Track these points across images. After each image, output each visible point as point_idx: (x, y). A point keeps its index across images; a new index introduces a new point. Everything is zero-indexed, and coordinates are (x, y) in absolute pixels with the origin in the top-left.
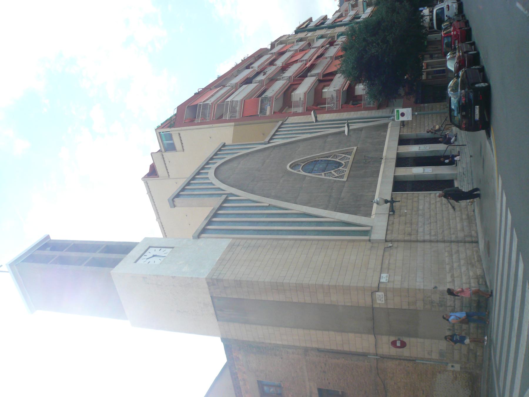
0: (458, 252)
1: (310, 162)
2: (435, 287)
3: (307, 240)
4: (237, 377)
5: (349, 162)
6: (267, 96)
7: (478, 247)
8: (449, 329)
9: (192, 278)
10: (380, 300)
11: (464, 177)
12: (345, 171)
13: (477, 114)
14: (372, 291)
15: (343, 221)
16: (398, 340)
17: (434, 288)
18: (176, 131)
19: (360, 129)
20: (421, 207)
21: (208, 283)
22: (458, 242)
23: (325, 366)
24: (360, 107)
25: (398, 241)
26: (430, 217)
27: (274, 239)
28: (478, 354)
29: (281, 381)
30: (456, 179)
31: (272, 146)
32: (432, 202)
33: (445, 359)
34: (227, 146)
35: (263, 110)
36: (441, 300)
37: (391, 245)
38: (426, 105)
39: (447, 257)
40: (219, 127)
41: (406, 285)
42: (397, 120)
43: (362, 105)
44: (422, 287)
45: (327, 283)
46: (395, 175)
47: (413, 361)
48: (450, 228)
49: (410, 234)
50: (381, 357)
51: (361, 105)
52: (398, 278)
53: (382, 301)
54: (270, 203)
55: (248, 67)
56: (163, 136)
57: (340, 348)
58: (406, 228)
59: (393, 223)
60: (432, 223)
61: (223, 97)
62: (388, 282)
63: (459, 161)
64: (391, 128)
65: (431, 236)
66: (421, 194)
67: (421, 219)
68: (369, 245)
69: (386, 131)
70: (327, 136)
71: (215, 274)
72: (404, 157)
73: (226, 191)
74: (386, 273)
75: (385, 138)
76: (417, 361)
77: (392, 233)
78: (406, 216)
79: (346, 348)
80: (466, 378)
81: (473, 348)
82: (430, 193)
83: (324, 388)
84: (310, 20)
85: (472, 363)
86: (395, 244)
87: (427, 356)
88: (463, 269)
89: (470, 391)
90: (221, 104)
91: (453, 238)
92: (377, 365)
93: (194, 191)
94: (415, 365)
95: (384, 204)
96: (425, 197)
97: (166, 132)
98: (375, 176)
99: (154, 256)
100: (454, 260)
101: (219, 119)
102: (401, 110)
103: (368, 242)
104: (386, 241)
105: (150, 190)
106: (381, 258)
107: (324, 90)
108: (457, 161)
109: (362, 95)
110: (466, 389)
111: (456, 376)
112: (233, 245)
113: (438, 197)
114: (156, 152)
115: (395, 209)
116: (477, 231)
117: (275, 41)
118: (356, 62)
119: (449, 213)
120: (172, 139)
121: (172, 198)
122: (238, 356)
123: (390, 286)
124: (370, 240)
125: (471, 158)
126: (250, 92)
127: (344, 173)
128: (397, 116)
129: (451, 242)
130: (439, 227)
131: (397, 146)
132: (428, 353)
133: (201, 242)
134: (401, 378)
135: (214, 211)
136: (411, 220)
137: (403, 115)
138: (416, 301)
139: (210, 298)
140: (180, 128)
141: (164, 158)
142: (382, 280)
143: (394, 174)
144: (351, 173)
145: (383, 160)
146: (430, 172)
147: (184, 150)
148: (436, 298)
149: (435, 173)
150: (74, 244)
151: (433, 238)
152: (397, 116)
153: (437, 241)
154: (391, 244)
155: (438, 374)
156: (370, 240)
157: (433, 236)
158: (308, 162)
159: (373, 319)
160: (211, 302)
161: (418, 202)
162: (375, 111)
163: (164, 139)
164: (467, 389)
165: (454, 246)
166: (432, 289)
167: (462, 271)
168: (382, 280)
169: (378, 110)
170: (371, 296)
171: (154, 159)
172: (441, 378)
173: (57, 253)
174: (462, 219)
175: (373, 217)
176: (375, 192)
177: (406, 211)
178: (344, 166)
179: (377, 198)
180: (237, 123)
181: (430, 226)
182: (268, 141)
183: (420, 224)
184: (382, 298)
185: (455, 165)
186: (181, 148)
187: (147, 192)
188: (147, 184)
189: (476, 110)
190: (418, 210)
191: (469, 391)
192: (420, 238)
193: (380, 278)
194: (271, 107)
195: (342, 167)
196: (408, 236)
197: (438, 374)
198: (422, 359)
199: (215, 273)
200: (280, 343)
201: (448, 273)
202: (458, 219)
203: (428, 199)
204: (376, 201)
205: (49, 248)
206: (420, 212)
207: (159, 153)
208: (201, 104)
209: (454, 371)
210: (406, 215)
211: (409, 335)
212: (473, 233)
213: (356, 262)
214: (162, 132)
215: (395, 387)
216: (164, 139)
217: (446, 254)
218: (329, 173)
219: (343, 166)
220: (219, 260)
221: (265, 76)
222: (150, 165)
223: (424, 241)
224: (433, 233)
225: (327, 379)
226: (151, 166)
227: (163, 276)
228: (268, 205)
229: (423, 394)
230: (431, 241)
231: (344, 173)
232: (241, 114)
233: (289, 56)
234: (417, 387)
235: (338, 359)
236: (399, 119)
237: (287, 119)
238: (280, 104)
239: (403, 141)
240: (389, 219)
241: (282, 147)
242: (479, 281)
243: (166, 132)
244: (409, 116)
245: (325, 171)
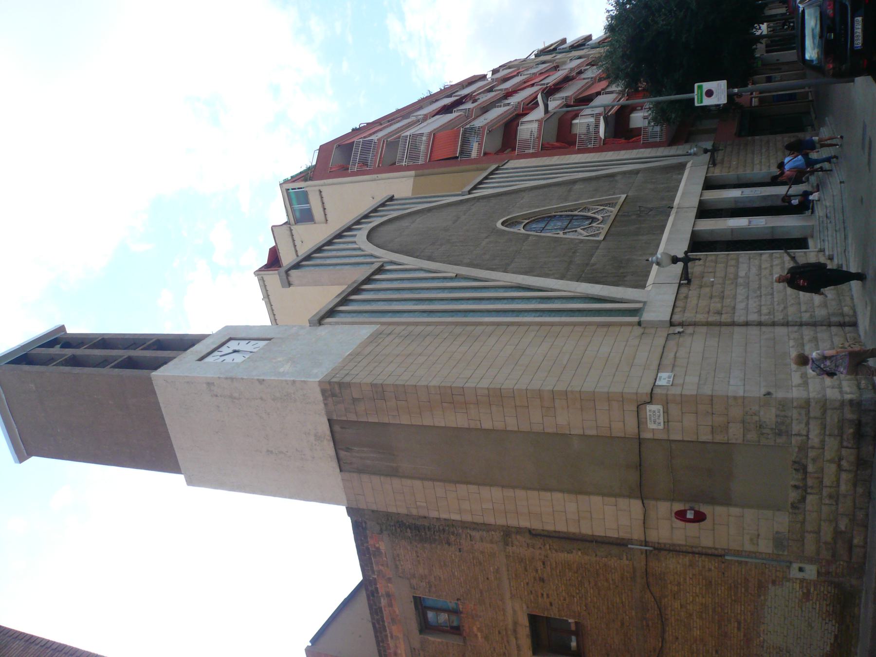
1: (540, 218)
2: (769, 394)
3: (519, 324)
4: (377, 589)
6: (473, 125)
7: (857, 331)
8: (796, 487)
9: (294, 382)
10: (655, 422)
11: (829, 222)
12: (602, 229)
13: (858, 34)
14: (639, 403)
15: (590, 296)
16: (689, 510)
17: (765, 395)
18: (315, 186)
20: (742, 273)
21: (323, 392)
23: (544, 568)
24: (637, 141)
27: (457, 324)
28: (856, 541)
29: (458, 600)
30: (812, 237)
32: (763, 266)
33: (786, 553)
34: (397, 200)
35: (465, 152)
36: (779, 420)
37: (681, 330)
38: (757, 137)
39: (793, 347)
40: (389, 179)
41: (707, 390)
42: (698, 103)
43: (641, 138)
44: (741, 393)
45: (550, 388)
46: (694, 229)
47: (720, 558)
48: (799, 304)
49: (719, 313)
50: (655, 548)
51: (639, 139)
55: (450, 96)
56: (293, 196)
57: (573, 529)
58: (712, 305)
59: (686, 297)
60: (763, 297)
62: (672, 385)
63: (818, 202)
64: (690, 169)
65: (761, 315)
68: (638, 331)
69: (683, 174)
70: (574, 182)
71: (337, 375)
72: (713, 208)
73: (382, 258)
76: (727, 558)
77: (684, 310)
78: (713, 286)
79: (586, 529)
80: (829, 595)
81: (846, 528)
82: (761, 254)
83: (542, 615)
84: (564, 41)
85: (842, 563)
86: (690, 330)
87: (748, 547)
89: (837, 625)
90: (392, 144)
91: (806, 317)
92: (646, 565)
94: (723, 566)
96: (750, 259)
97: (299, 188)
99: (235, 351)
101: (393, 167)
102: (707, 86)
103: (636, 328)
104: (672, 324)
105: (267, 293)
106: (660, 350)
107: (575, 122)
108: (815, 202)
109: (641, 128)
110: (827, 620)
111: (809, 591)
112: (380, 334)
113: (776, 281)
114: (281, 225)
116: (854, 306)
117: (500, 67)
118: (629, 45)
120: (307, 202)
122: (377, 545)
123: (676, 391)
124: (639, 324)
126: (446, 123)
128: (698, 97)
129: (801, 324)
130: (777, 302)
131: (701, 191)
132: (751, 540)
133: (323, 331)
134: (694, 594)
135: (355, 285)
136: (723, 292)
137: (709, 93)
138: (729, 423)
140: (322, 182)
141: (292, 235)
142: (658, 383)
143: (693, 228)
144: (613, 229)
145: (673, 209)
146: (762, 224)
147: (327, 220)
148: (769, 416)
149: (771, 225)
150: (103, 339)
151: (764, 318)
152: (699, 98)
153: (774, 324)
154: (682, 328)
155: (770, 586)
156: (639, 324)
157: (766, 315)
159: (640, 465)
160: (328, 433)
162: (663, 148)
163: (294, 202)
164: (829, 620)
165: (808, 332)
166: (762, 396)
168: (658, 383)
169: (670, 147)
170: (636, 413)
171: (276, 238)
172: (776, 595)
173: (69, 352)
175: (648, 288)
178: (601, 222)
180: (420, 172)
181: (760, 301)
183: (740, 298)
184: (659, 416)
185: (810, 211)
186: (323, 219)
187: (263, 297)
188: (264, 281)
189: (857, 27)
190: (736, 276)
191: (834, 623)
192: (740, 317)
193: (656, 380)
194: (480, 144)
196: (715, 315)
197: (770, 586)
198: (738, 553)
199: (337, 374)
200: (455, 517)
201: (794, 371)
205: (59, 346)
206: (740, 280)
207: (285, 226)
208: (360, 140)
209: (804, 579)
210: (712, 285)
211: (713, 501)
212: (846, 309)
214: (292, 189)
215: (683, 613)
216: (294, 202)
217: (792, 343)
220: (349, 355)
221: (476, 104)
222: (270, 249)
223: (747, 324)
224: (765, 310)
225: (548, 596)
226: (270, 249)
227: (242, 379)
228: (455, 275)
229: (739, 629)
230: (760, 324)
232: (427, 157)
233: (519, 80)
234: (726, 615)
235: (568, 553)
236: (702, 102)
237: (507, 163)
238: (498, 142)
239: (709, 185)
240: (680, 292)
241: (492, 198)
242: (860, 383)
243: (299, 188)
244: (723, 96)
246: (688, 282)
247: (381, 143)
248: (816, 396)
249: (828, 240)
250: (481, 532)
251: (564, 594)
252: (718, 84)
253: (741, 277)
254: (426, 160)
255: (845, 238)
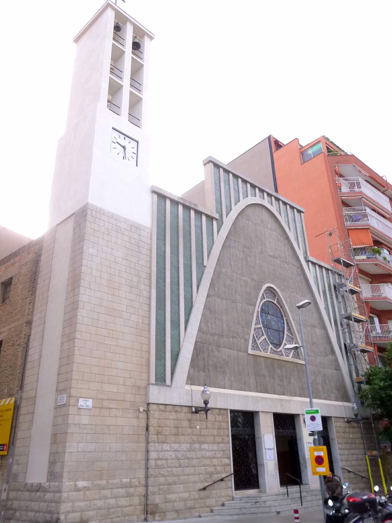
0: (129, 495)
5: (282, 356)
19: (338, 368)
20: (205, 446)
22: (146, 496)
25: (148, 418)
26: (188, 458)
30: (260, 492)
31: (301, 265)
32: (213, 460)
39: (121, 481)
44: (67, 450)
52: (85, 420)
53: (59, 403)
54: (207, 268)
59: (176, 411)
60: (178, 461)
61: (368, 200)
66: (228, 446)
67: (185, 446)
69: (337, 400)
70: (324, 327)
72: (296, 424)
74: (92, 405)
75: (326, 399)
77: (160, 410)
82: (229, 458)
86: (143, 416)
88: (99, 503)
93: (284, 211)
95: (203, 400)
98: (259, 387)
99: (124, 147)
100: (115, 491)
103: (146, 382)
115: (202, 414)
119: (195, 482)
121: (213, 161)
123: (72, 410)
125: (276, 513)
127: (262, 350)
129: (147, 486)
131: (272, 411)
136: (183, 435)
139: (73, 213)
143: (262, 412)
144: (263, 359)
151: (152, 463)
152: (310, 412)
153: (147, 468)
154: (144, 410)
157: (156, 463)
158: (280, 308)
161: (214, 443)
165: (142, 490)
167: (96, 502)
174: (185, 500)
175: (188, 387)
176: (231, 388)
177: (198, 427)
179: (211, 390)
181: (172, 459)
182: (310, 260)
183: (176, 446)
184: (62, 402)
190: (201, 443)
192: (152, 447)
195: (272, 347)
202: (186, 495)
203: (219, 455)
204: (206, 389)
206: (197, 446)
213: (113, 369)
218: (263, 333)
219: (275, 349)
223: (148, 451)
224: (159, 462)
225: (8, 349)
230: (147, 460)
231: (262, 350)
245: (266, 329)
246: (193, 412)
247: (359, 194)
248: (63, 497)
249: (237, 503)
250: (32, 308)
251: (8, 357)
252: (320, 424)
253: (200, 446)
254: (348, 227)
255: (230, 515)
